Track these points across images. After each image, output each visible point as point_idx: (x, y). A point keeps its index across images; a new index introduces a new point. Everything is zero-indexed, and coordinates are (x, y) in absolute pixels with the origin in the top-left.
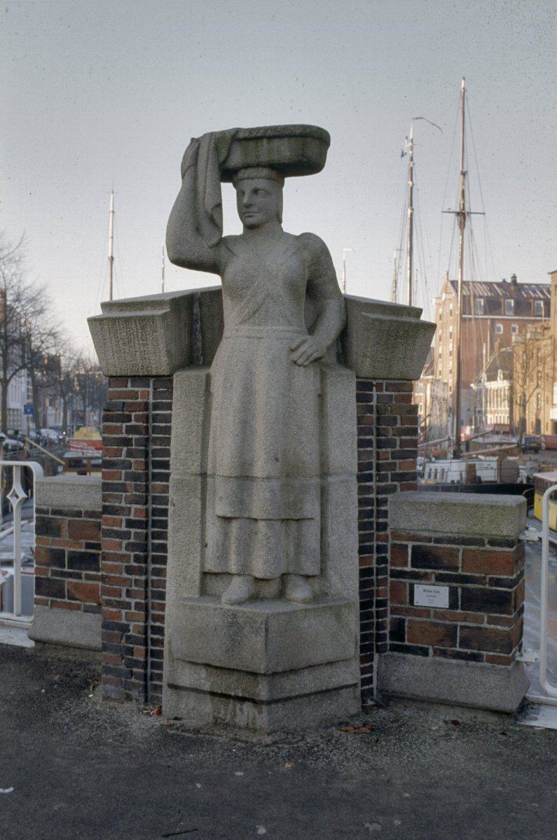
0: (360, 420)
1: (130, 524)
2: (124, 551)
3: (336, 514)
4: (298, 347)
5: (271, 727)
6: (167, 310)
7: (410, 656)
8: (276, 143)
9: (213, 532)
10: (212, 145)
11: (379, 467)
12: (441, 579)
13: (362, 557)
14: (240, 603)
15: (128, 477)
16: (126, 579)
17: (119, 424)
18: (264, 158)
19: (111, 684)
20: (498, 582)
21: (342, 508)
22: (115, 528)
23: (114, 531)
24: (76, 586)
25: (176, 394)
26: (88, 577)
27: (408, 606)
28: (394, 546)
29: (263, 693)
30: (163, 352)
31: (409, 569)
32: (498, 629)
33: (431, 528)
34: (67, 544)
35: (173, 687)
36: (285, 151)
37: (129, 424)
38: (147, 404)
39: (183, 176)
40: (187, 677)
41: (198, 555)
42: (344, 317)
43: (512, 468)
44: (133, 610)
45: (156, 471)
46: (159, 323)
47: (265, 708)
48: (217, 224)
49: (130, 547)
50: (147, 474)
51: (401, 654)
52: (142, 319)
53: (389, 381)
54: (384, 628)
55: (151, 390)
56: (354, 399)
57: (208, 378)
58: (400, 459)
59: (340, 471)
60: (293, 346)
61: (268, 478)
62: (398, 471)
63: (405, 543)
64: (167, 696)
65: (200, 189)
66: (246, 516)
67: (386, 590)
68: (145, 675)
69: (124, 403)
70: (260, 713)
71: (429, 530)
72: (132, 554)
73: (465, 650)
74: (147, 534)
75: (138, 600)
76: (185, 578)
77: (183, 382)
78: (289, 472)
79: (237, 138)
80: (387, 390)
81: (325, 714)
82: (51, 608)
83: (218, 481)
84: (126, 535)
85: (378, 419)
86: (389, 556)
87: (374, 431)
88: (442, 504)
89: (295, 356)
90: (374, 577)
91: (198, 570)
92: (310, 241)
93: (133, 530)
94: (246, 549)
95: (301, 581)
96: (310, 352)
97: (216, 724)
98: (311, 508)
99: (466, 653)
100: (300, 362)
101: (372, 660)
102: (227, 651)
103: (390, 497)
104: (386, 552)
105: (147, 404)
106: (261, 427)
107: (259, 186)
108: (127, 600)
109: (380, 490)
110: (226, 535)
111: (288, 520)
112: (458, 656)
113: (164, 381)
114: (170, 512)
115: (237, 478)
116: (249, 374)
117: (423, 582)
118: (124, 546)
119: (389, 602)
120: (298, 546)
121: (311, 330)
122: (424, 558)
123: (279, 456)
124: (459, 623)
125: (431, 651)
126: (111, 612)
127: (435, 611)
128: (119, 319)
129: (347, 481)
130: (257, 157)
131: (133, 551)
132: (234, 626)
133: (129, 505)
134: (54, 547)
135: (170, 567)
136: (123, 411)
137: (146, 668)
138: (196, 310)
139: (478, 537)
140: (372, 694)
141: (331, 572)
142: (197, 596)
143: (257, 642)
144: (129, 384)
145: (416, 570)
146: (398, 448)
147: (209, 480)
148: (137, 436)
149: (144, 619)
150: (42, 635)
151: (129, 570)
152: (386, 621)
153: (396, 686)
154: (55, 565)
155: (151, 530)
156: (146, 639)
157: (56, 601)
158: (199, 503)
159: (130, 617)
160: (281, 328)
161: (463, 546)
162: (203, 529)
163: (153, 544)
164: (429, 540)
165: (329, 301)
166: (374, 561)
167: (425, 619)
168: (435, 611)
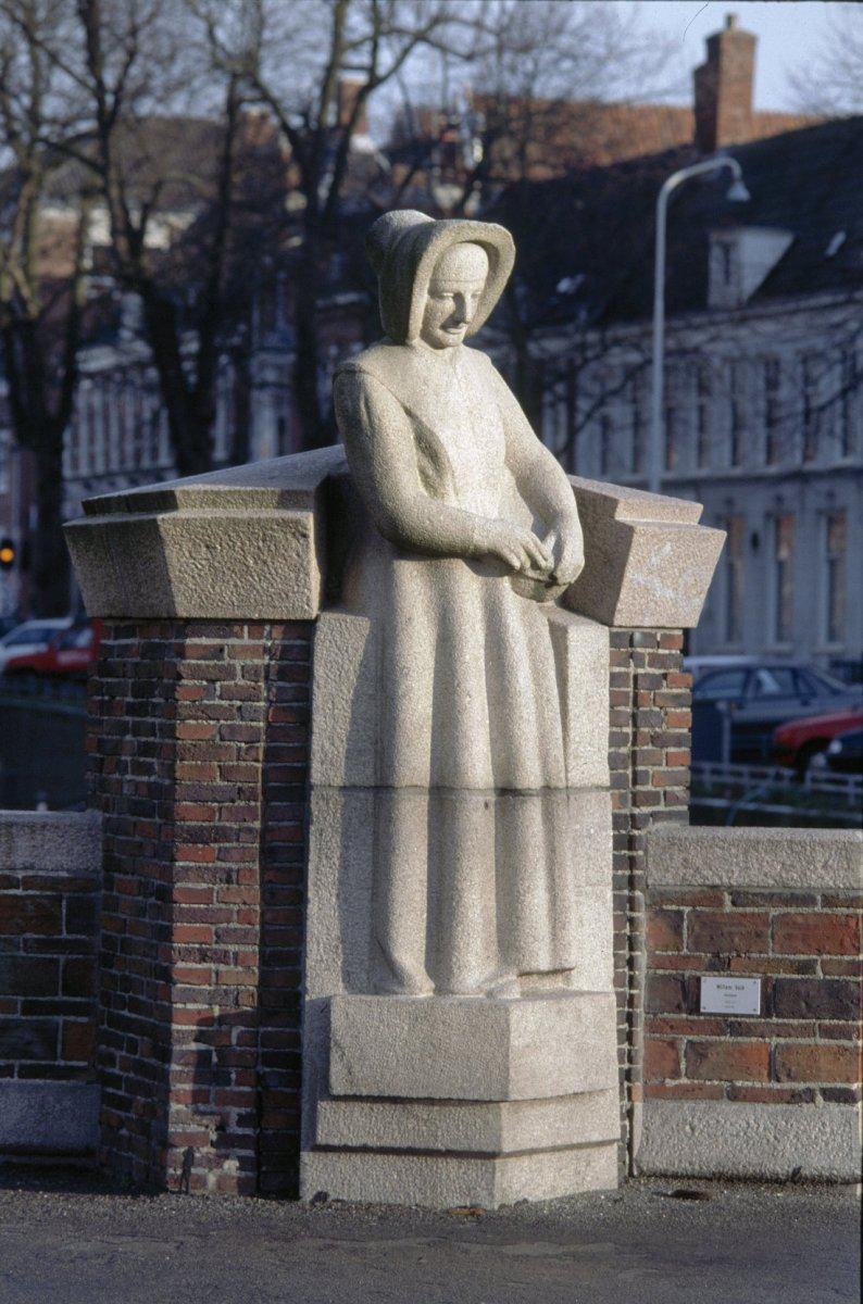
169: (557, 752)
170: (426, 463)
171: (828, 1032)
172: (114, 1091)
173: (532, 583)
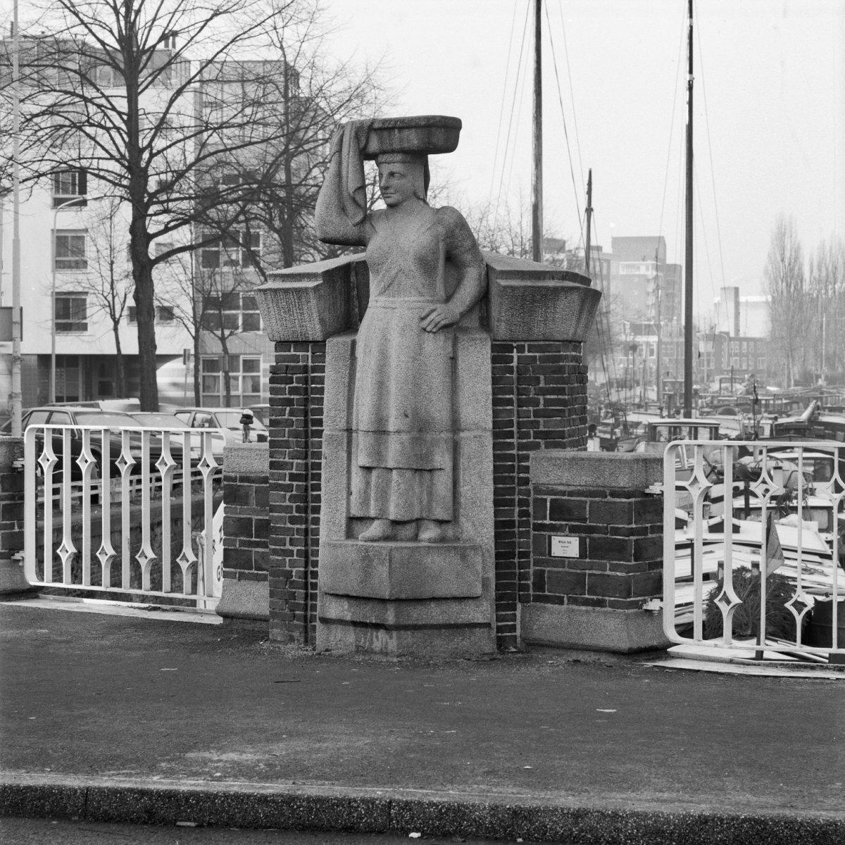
0: (495, 381)
1: (293, 477)
2: (287, 503)
3: (469, 466)
4: (428, 315)
5: (400, 651)
6: (320, 282)
7: (549, 605)
8: (406, 133)
9: (357, 480)
10: (353, 134)
11: (520, 425)
12: (574, 530)
14: (373, 540)
15: (291, 434)
16: (290, 528)
17: (283, 386)
18: (396, 146)
19: (276, 628)
20: (616, 531)
21: (474, 460)
22: (280, 482)
23: (280, 485)
24: (263, 555)
25: (328, 358)
27: (547, 557)
28: (536, 500)
29: (390, 618)
30: (317, 320)
31: (548, 522)
32: (617, 576)
33: (564, 482)
34: (255, 512)
36: (413, 139)
37: (291, 385)
38: (306, 367)
40: (335, 609)
41: (344, 502)
42: (483, 284)
43: (10, 373)
44: (295, 557)
45: (314, 428)
46: (311, 295)
47: (394, 634)
49: (292, 498)
50: (306, 432)
51: (542, 604)
52: (298, 290)
53: (532, 343)
54: (527, 579)
55: (310, 354)
56: (489, 361)
57: (354, 343)
58: (544, 417)
59: (473, 427)
60: (423, 315)
61: (398, 432)
62: (542, 428)
63: (545, 497)
64: (320, 632)
65: (344, 173)
66: (383, 466)
67: (529, 543)
68: (306, 616)
69: (287, 366)
70: (391, 638)
71: (563, 484)
72: (294, 505)
73: (592, 597)
74: (307, 486)
75: (299, 548)
76: (334, 523)
77: (335, 346)
78: (419, 426)
80: (529, 352)
81: (456, 648)
82: (239, 580)
83: (361, 434)
84: (289, 488)
85: (518, 379)
86: (531, 509)
87: (515, 390)
88: (573, 459)
90: (516, 530)
91: (344, 515)
92: (445, 216)
93: (295, 483)
94: (383, 496)
95: (432, 525)
96: (437, 319)
97: (357, 652)
98: (442, 459)
99: (593, 599)
100: (428, 329)
101: (515, 610)
102: (361, 582)
103: (532, 454)
104: (528, 506)
105: (306, 367)
106: (393, 386)
107: (394, 170)
108: (291, 548)
109: (521, 447)
110: (368, 483)
111: (421, 470)
112: (586, 603)
113: (319, 346)
114: (323, 465)
115: (374, 432)
116: (385, 340)
117: (559, 533)
118: (287, 497)
119: (532, 554)
120: (430, 494)
121: (448, 299)
122: (560, 510)
123: (409, 412)
124: (587, 572)
125: (565, 599)
126: (277, 560)
127: (569, 562)
128: (280, 289)
129: (480, 437)
130: (391, 145)
131: (295, 502)
132: (367, 559)
133: (291, 461)
134: (242, 516)
135: (323, 516)
136: (286, 373)
137: (306, 610)
138: (353, 279)
139: (601, 489)
140: (515, 641)
141: (463, 519)
142: (343, 538)
143: (382, 571)
144: (292, 349)
145: (554, 523)
146: (541, 407)
147: (354, 434)
148: (298, 397)
149: (304, 565)
150: (230, 608)
151: (293, 520)
152: (529, 572)
153: (537, 634)
154: (242, 535)
156: (306, 583)
157: (243, 573)
158: (345, 455)
159: (293, 564)
160: (413, 299)
161: (590, 499)
162: (349, 479)
163: (312, 495)
164: (563, 493)
165: (468, 269)
166: (516, 514)
167: (561, 569)
168: (569, 562)
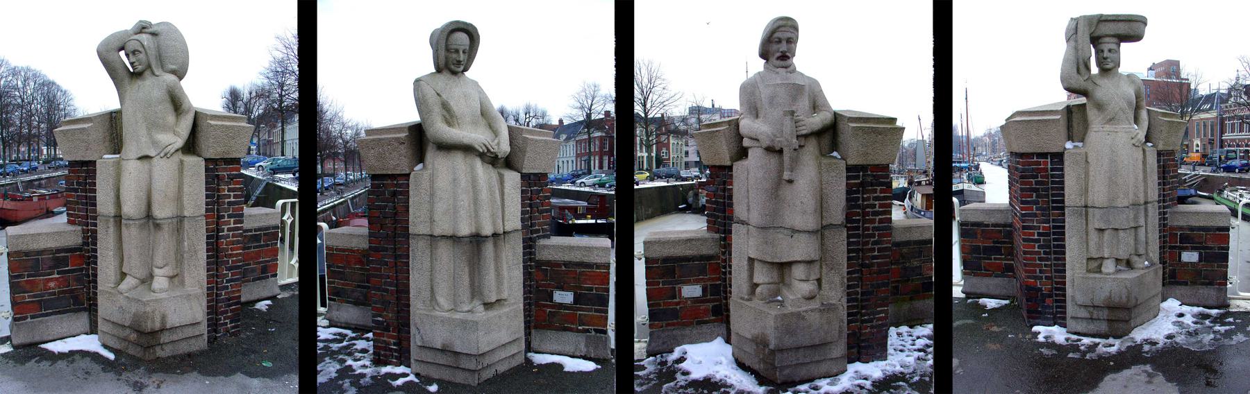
1: (1039, 234)
13: (963, 210)
26: (995, 259)
35: (1072, 318)
36: (1122, 29)
39: (1068, 41)
44: (1044, 280)
48: (1088, 68)
55: (1049, 160)
79: (1102, 20)
89: (1134, 141)
144: (1035, 158)
150: (968, 290)
151: (1040, 259)
155: (1052, 237)
169: (500, 221)
170: (445, 113)
171: (596, 311)
172: (868, 203)
173: (489, 158)
